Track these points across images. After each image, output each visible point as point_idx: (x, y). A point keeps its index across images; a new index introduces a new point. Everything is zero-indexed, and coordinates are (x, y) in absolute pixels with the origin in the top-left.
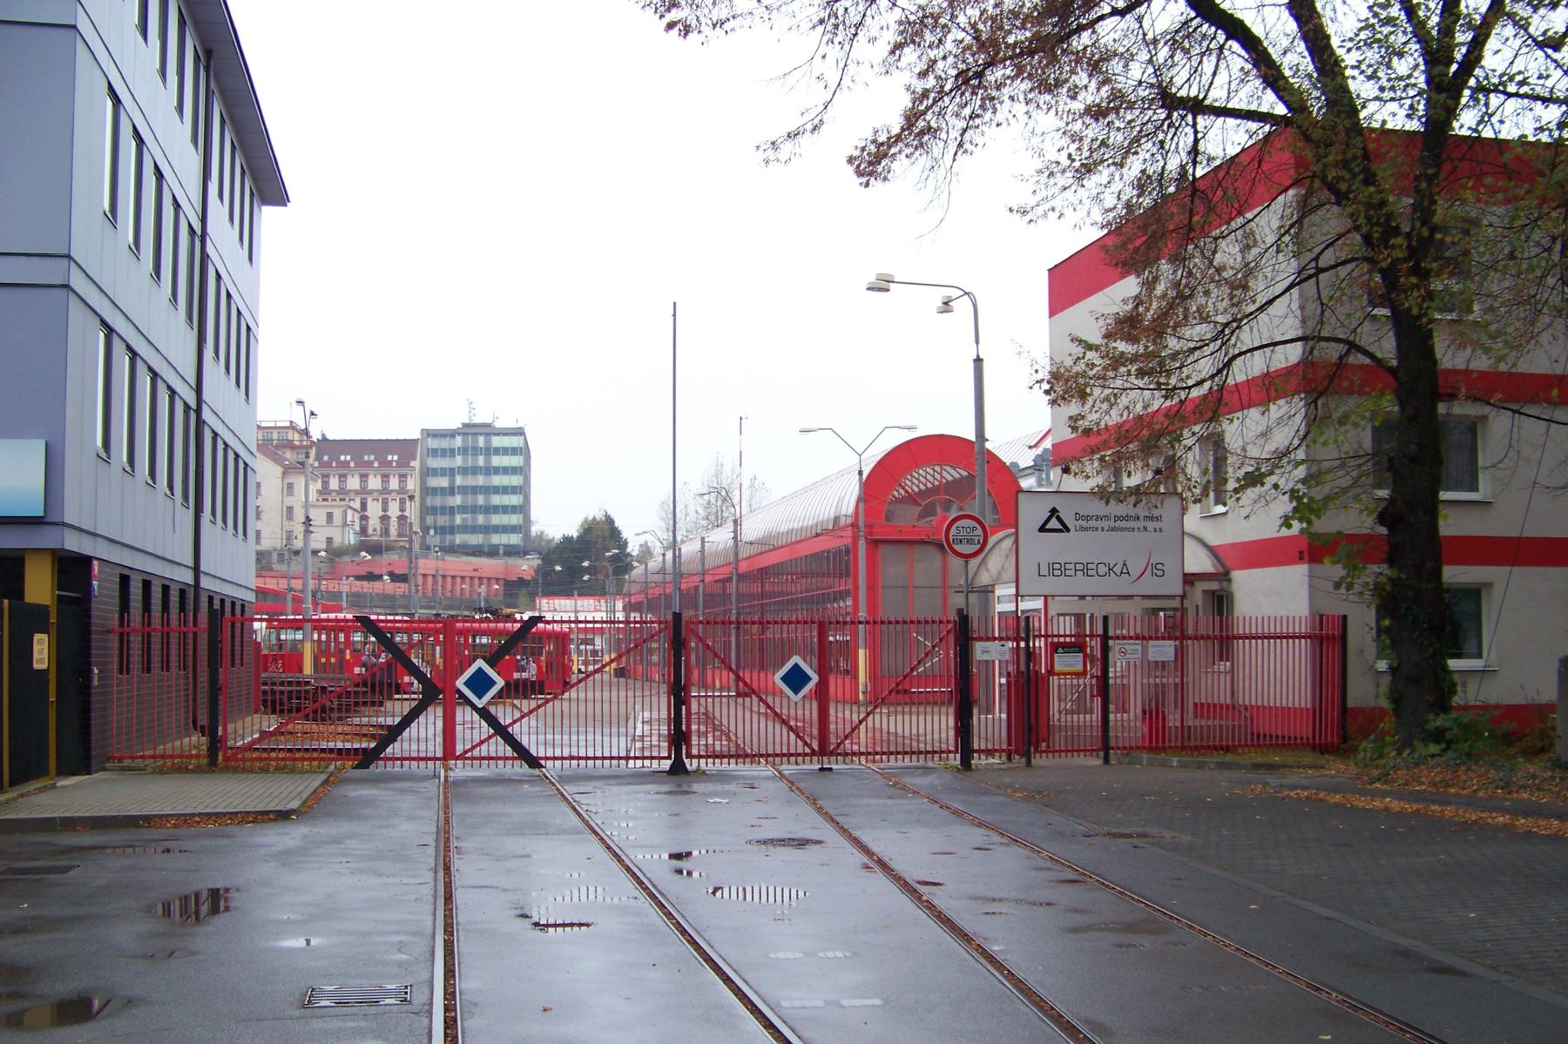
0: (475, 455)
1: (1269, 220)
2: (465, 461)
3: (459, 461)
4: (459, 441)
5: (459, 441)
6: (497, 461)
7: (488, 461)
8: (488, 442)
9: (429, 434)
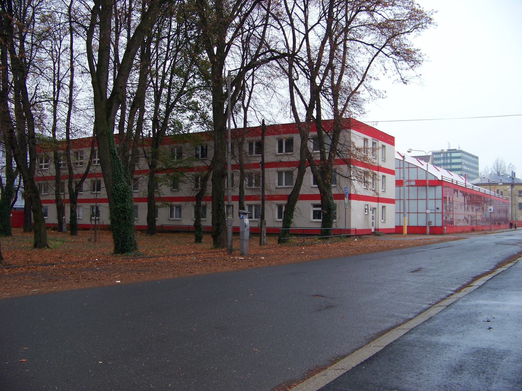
0: (447, 159)
1: (51, 136)
2: (444, 161)
3: (442, 161)
4: (442, 155)
5: (442, 155)
6: (454, 161)
7: (451, 161)
8: (451, 155)
9: (434, 153)
